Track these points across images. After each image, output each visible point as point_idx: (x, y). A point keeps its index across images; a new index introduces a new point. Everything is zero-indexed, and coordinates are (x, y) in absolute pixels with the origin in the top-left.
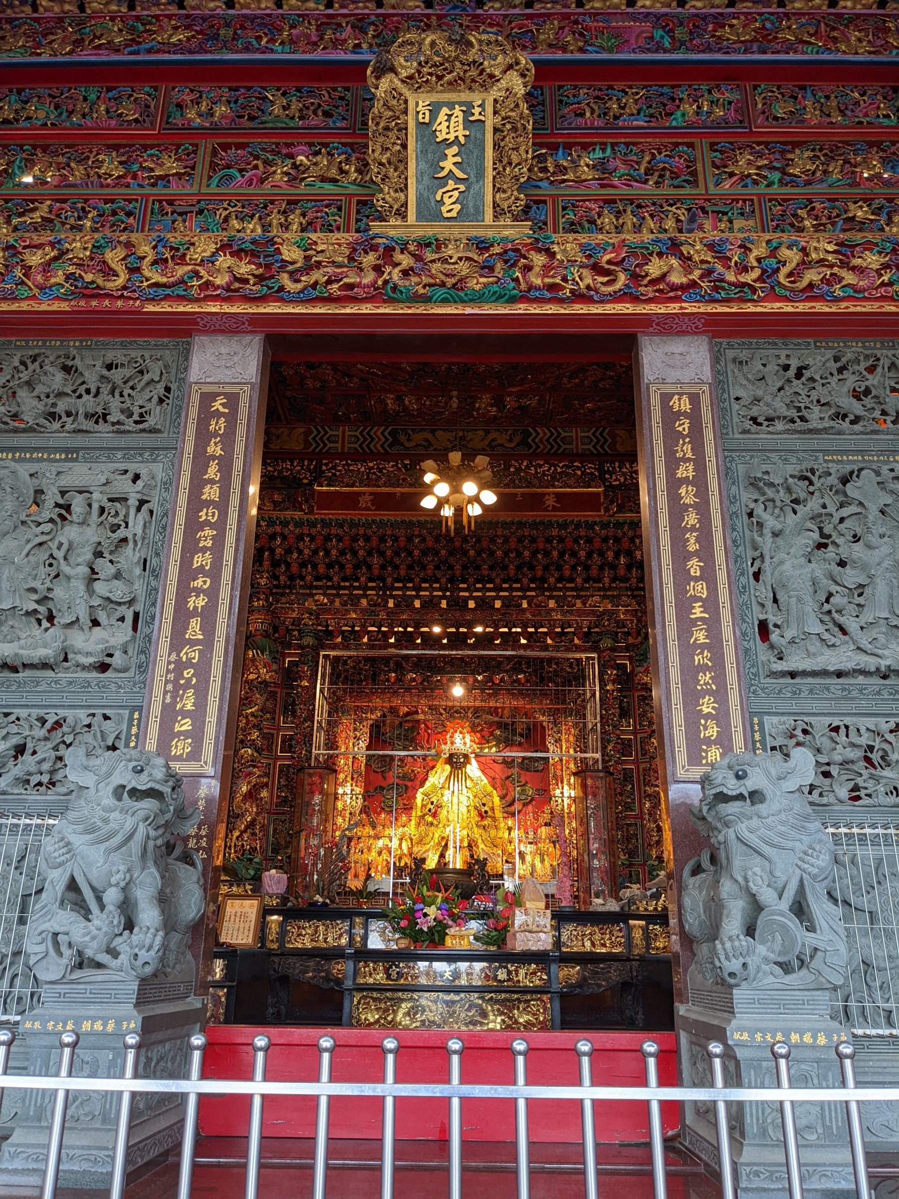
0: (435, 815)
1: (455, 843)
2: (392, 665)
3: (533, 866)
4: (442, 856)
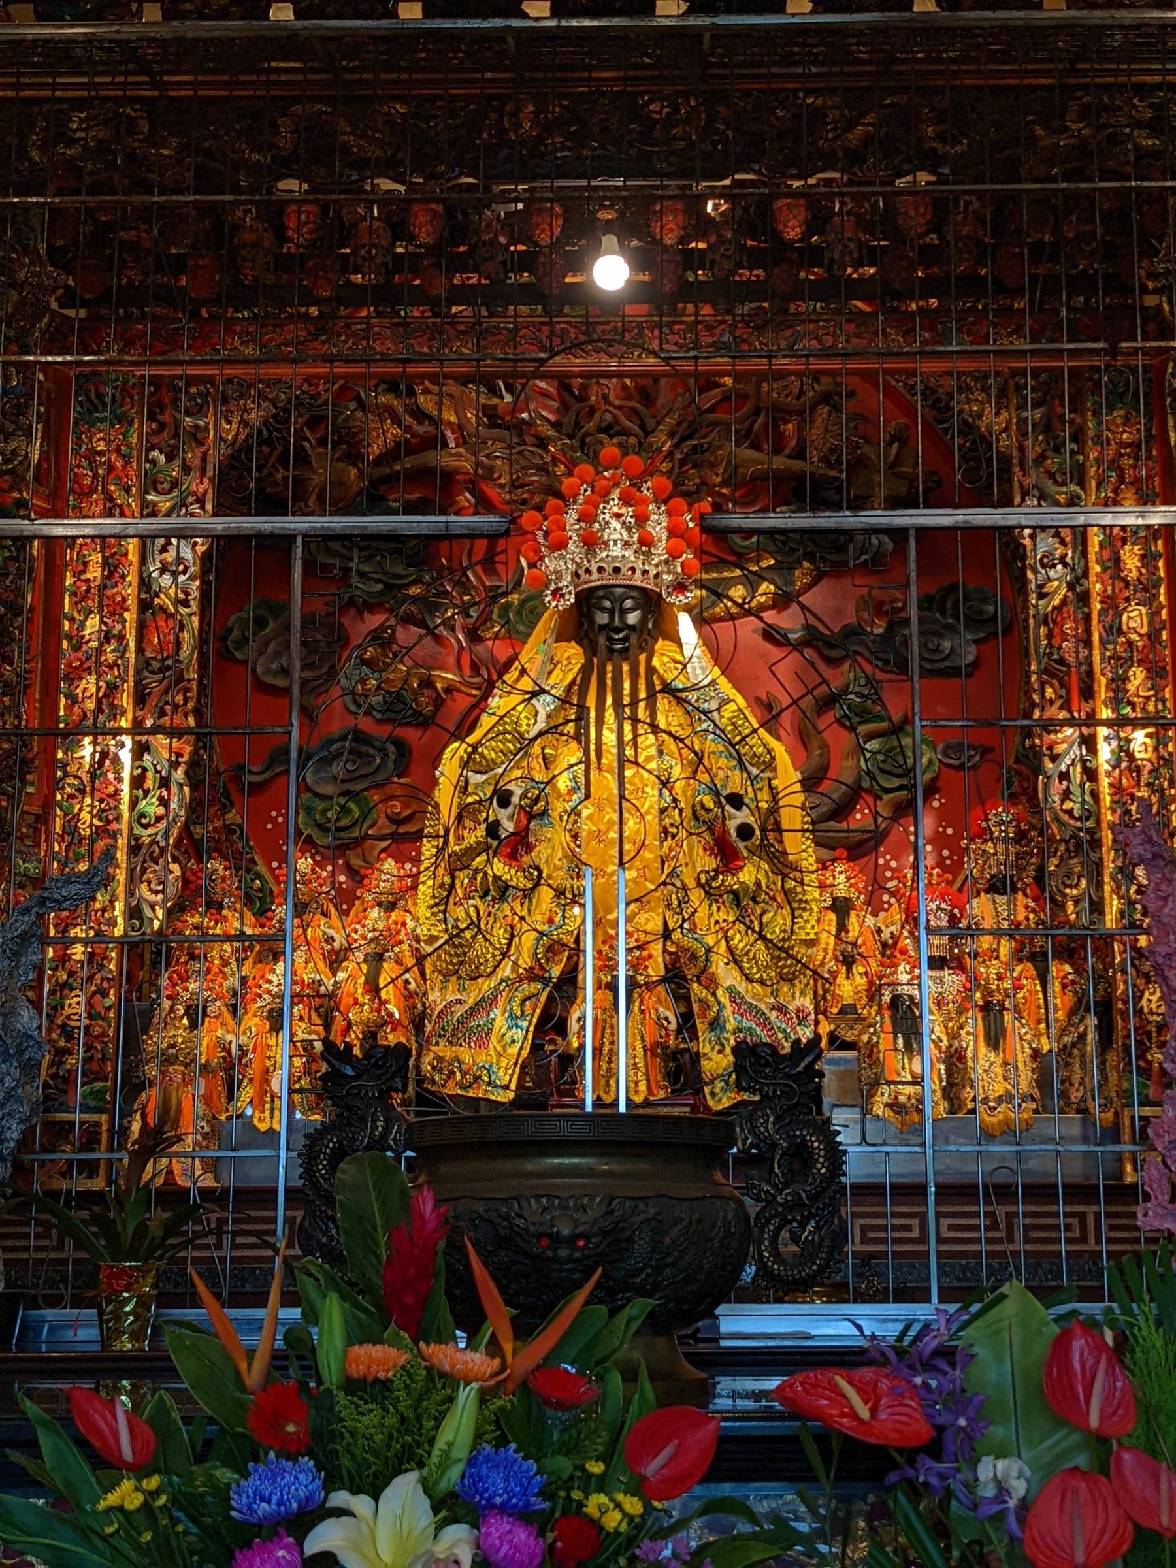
0: (517, 846)
1: (607, 964)
2: (285, 138)
3: (955, 1059)
4: (551, 1023)
